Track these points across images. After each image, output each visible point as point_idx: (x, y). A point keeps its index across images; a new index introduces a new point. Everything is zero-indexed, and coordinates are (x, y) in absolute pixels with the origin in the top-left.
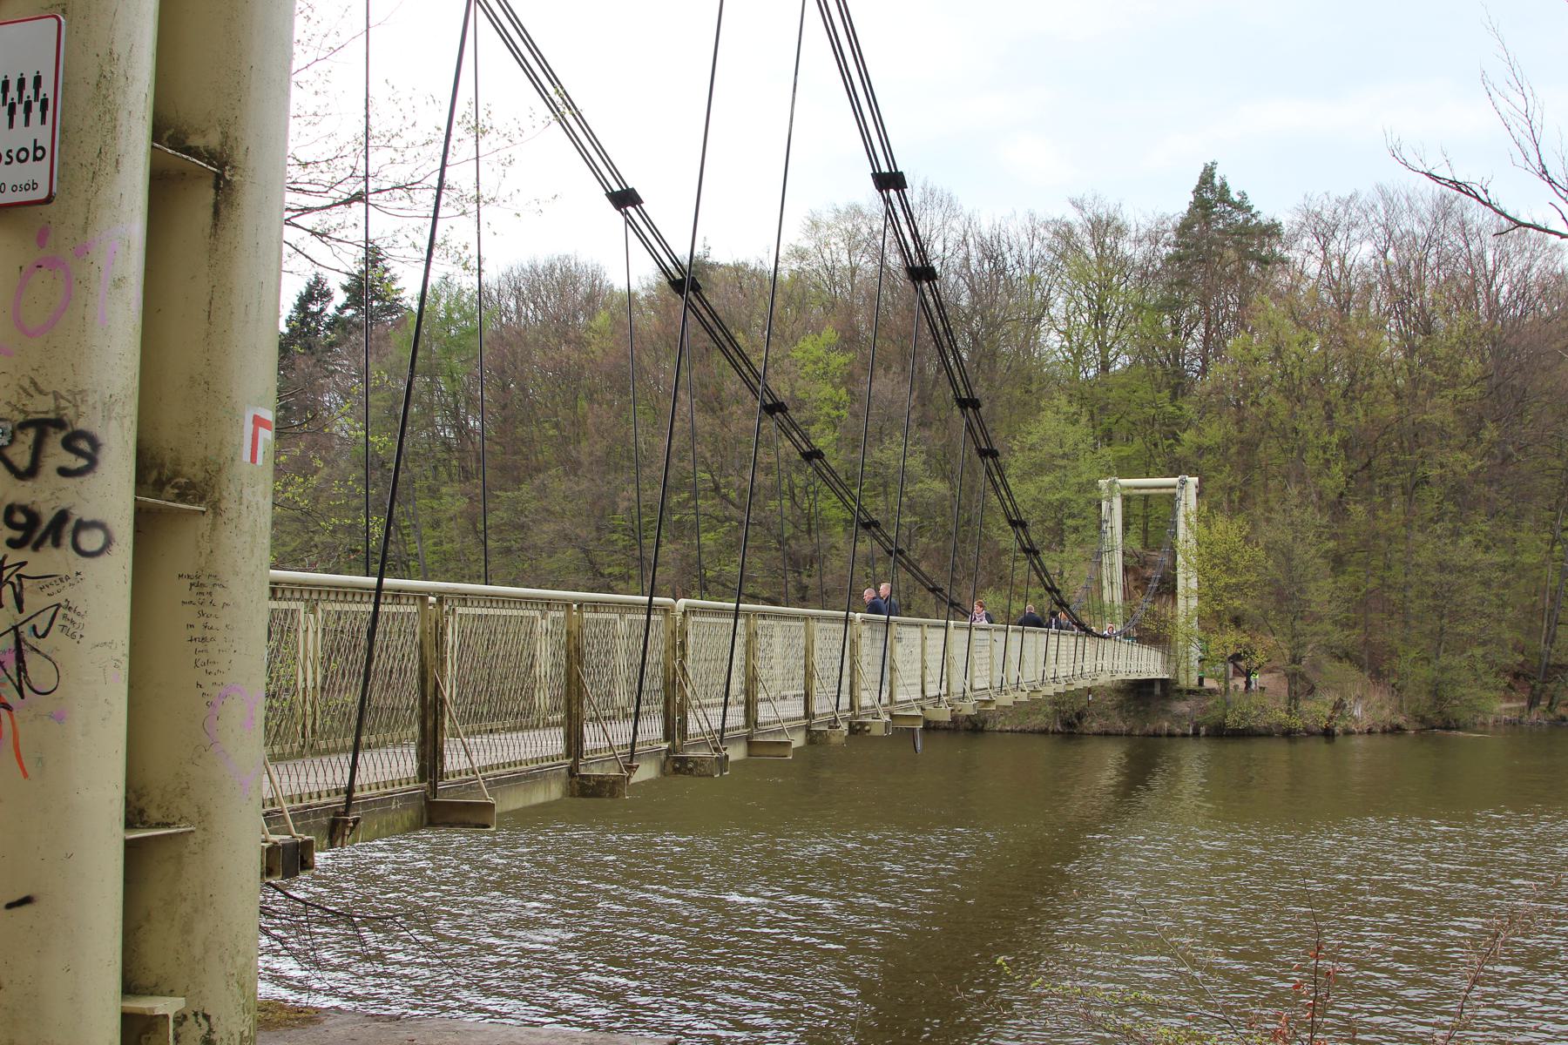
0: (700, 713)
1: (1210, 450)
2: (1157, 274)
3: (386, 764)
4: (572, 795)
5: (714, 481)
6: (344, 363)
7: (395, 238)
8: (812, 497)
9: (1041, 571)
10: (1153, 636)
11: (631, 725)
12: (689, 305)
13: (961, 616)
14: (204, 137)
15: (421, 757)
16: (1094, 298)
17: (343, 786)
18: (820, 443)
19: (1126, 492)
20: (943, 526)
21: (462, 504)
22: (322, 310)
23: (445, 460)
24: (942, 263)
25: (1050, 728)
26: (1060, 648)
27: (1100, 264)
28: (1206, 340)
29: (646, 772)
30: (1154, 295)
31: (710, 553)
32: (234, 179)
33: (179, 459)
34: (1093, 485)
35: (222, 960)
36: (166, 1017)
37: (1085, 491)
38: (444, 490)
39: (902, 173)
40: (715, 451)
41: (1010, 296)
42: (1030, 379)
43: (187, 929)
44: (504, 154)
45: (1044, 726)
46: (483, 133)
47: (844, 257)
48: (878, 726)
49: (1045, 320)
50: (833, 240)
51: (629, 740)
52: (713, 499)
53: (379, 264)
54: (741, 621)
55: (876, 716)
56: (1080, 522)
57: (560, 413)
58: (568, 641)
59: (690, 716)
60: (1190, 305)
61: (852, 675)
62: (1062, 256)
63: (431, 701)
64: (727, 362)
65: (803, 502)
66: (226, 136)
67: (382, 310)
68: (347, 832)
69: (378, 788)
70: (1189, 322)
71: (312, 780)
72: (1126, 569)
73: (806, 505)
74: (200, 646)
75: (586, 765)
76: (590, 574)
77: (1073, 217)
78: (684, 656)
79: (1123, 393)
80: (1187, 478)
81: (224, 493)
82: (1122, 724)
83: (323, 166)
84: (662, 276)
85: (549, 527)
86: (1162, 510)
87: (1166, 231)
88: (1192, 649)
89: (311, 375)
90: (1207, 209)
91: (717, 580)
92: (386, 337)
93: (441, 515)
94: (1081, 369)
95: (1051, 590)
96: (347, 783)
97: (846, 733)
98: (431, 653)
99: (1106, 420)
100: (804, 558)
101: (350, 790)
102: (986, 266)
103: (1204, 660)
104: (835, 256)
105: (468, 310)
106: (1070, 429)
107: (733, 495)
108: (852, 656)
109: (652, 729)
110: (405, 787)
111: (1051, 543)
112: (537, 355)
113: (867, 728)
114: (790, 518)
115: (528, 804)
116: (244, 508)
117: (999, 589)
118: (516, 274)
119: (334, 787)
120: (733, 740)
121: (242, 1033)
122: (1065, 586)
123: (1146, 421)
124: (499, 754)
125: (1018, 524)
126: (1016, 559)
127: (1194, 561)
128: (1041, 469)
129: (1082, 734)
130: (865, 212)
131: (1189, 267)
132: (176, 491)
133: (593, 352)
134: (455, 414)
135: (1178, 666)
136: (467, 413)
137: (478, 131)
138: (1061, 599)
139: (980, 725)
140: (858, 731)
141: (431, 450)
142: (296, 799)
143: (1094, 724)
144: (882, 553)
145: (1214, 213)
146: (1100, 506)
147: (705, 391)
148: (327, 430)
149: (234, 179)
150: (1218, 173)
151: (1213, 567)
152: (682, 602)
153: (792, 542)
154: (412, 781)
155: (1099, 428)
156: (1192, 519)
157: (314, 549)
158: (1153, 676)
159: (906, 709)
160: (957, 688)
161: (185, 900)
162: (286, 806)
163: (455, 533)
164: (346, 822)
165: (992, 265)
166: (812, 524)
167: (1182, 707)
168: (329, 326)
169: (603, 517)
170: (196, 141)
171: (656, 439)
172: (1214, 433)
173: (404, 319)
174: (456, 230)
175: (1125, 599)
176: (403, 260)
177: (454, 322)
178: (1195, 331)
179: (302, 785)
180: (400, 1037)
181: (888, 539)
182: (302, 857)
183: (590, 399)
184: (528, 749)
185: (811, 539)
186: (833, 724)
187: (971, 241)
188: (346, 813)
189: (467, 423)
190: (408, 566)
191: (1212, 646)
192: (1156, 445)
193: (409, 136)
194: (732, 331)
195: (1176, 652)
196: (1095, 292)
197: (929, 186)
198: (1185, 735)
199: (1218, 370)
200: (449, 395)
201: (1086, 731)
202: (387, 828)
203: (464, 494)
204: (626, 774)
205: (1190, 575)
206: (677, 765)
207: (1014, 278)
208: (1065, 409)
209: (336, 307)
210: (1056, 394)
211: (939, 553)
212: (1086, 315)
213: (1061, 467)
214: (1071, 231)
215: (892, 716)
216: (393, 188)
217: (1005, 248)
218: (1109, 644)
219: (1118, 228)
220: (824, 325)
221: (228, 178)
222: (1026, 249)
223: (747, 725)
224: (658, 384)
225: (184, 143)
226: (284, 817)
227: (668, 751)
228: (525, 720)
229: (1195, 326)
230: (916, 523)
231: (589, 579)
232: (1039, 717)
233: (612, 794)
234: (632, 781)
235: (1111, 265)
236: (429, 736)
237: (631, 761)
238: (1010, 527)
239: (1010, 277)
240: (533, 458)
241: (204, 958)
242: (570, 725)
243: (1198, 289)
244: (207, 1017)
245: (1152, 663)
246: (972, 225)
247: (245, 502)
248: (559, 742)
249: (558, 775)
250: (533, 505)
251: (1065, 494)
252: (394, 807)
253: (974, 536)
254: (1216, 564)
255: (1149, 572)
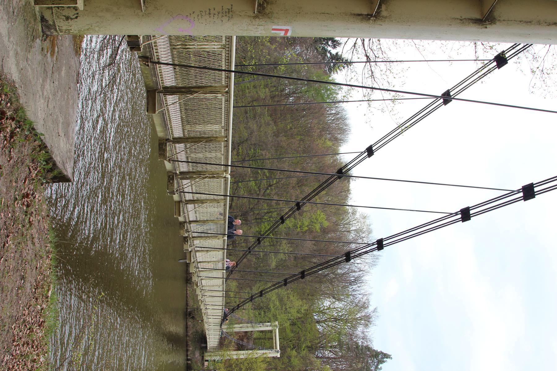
0: (190, 184)
1: (290, 360)
2: (352, 339)
3: (169, 75)
4: (159, 140)
5: (273, 185)
6: (310, 54)
7: (354, 72)
8: (268, 219)
9: (244, 303)
10: (223, 343)
11: (185, 160)
12: (333, 176)
13: (228, 274)
14: (385, 10)
15: (172, 87)
16: (342, 317)
17: (160, 60)
18: (287, 222)
19: (274, 331)
20: (259, 266)
21: (262, 96)
22: (329, 45)
23: (278, 90)
24: (353, 263)
25: (188, 307)
26: (216, 310)
27: (354, 319)
28: (329, 358)
29: (168, 166)
30: (344, 338)
31: (247, 184)
32: (371, 21)
33: (273, 4)
34: (276, 319)
35: (97, 22)
36: (76, 4)
37: (273, 317)
38: (267, 90)
39: (383, 249)
40: (283, 185)
41: (342, 287)
42: (313, 296)
43: (108, 10)
44: (385, 109)
45: (189, 305)
46: (393, 102)
47: (353, 228)
48: (187, 247)
49: (334, 300)
50: (359, 224)
51: (179, 160)
52: (267, 185)
53: (346, 65)
54: (222, 197)
55: (191, 246)
56: (263, 315)
57: (295, 129)
58: (214, 137)
59: (189, 181)
60: (341, 352)
61: (205, 237)
62: (357, 305)
63: (191, 90)
64: (315, 188)
65: (266, 216)
66: (386, 17)
67: (330, 66)
68: (144, 62)
69: (160, 73)
70: (335, 351)
71: (162, 50)
72: (246, 332)
73: (265, 217)
74: (207, 12)
75: (170, 145)
76: (239, 142)
77: (371, 309)
78: (210, 178)
79: (309, 329)
80: (279, 353)
81: (261, 20)
82: (191, 333)
83: (379, 47)
84: (345, 164)
85: (255, 127)
86: (268, 344)
87: (367, 342)
88: (218, 357)
89: (306, 42)
90: (375, 356)
91: (238, 186)
92: (320, 68)
93: (258, 89)
94: (317, 313)
95: (238, 306)
96: (162, 62)
97: (184, 236)
98: (208, 89)
99: (299, 323)
100: (247, 218)
101: (159, 63)
102: (352, 279)
103: (215, 362)
104: (354, 225)
105: (331, 96)
106: (296, 310)
107: (268, 191)
108: (211, 237)
109: (184, 168)
110: (161, 82)
111: (255, 305)
112: (315, 121)
113: (186, 243)
114: (261, 212)
115: (156, 125)
116: (256, 26)
117: (238, 287)
118: (344, 113)
119: (160, 57)
120: (180, 196)
121: (71, 30)
122: (239, 311)
123: (299, 338)
124: (173, 114)
125: (261, 294)
126: (248, 293)
127: (250, 357)
128: (281, 300)
129: (187, 319)
130: (370, 235)
131: (355, 351)
132: (262, 3)
133: (317, 141)
134: (294, 93)
135: (212, 352)
136: (294, 97)
137: (393, 100)
138: (235, 310)
139: (189, 282)
140: (185, 240)
141: (281, 85)
142: (155, 44)
143: (190, 323)
144: (250, 245)
145: (374, 359)
146: (268, 322)
147: (305, 181)
148: (286, 49)
149: (371, 21)
150: (388, 360)
151: (248, 364)
152: (229, 176)
153: (252, 213)
154: (163, 84)
155: (296, 321)
156: (265, 356)
157: (245, 44)
158: (208, 343)
159: (193, 256)
160: (202, 274)
161: (118, 9)
162: (153, 41)
163: (252, 94)
164: (148, 62)
165: (353, 280)
166: (259, 220)
167: (197, 354)
168: (323, 48)
169: (259, 145)
170: (384, 7)
171: (287, 164)
172: (296, 362)
173: (327, 74)
174: (357, 94)
175: (236, 332)
176: (347, 75)
177: (326, 91)
178: (332, 353)
179: (160, 46)
180: (71, 84)
181: (254, 247)
182: (135, 47)
183: (301, 140)
184: (175, 124)
185: (253, 220)
186: (187, 231)
187: (361, 273)
188: (151, 62)
189: (291, 97)
190: (240, 77)
191: (220, 364)
192: (291, 341)
193: (391, 76)
194: (326, 189)
195: (217, 351)
196: (344, 317)
197: (380, 257)
198: (187, 356)
199: (319, 361)
200: (301, 90)
201: (188, 320)
202: (146, 76)
203: (266, 97)
204: (168, 159)
205: (245, 355)
206: (171, 177)
207: (348, 289)
208: (302, 309)
209: (330, 50)
210: (307, 305)
211: (250, 265)
212: (336, 315)
213: (282, 308)
214: (365, 308)
215: (191, 252)
216: (372, 71)
217: (359, 285)
218: (218, 328)
219: (367, 325)
220: (330, 222)
221: (371, 19)
222: (359, 292)
223: (186, 201)
224: (306, 164)
225: (383, 3)
226: (149, 41)
227: (176, 173)
228: (185, 121)
229: (333, 354)
230: (260, 257)
231: (237, 141)
232: (192, 303)
233: (160, 154)
234: (165, 161)
235: (354, 323)
236: (178, 90)
237: (172, 161)
238: (260, 290)
239: (349, 287)
240: (279, 121)
241: (97, 16)
242: (184, 139)
243: (347, 354)
244: (76, 18)
245: (213, 343)
246: (367, 273)
247: (259, 27)
248: (178, 135)
249: (166, 135)
250: (263, 121)
251: (273, 310)
252: (153, 78)
253: (256, 278)
254: (249, 365)
255: (245, 340)
